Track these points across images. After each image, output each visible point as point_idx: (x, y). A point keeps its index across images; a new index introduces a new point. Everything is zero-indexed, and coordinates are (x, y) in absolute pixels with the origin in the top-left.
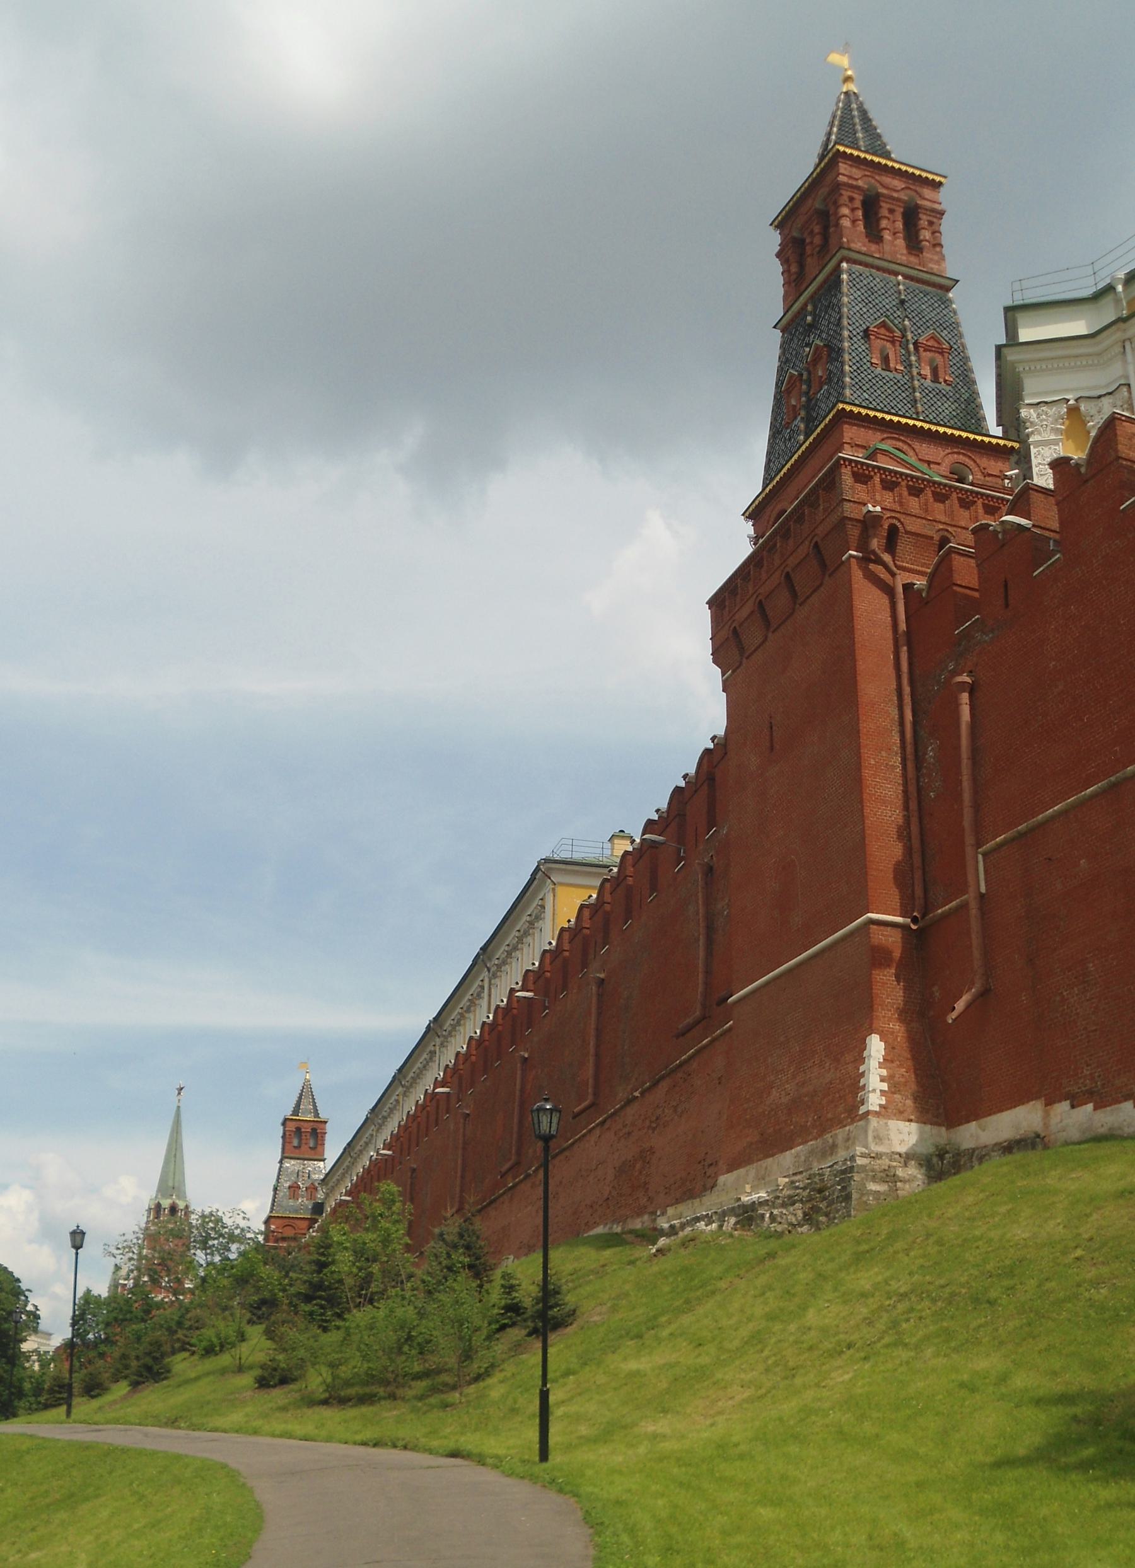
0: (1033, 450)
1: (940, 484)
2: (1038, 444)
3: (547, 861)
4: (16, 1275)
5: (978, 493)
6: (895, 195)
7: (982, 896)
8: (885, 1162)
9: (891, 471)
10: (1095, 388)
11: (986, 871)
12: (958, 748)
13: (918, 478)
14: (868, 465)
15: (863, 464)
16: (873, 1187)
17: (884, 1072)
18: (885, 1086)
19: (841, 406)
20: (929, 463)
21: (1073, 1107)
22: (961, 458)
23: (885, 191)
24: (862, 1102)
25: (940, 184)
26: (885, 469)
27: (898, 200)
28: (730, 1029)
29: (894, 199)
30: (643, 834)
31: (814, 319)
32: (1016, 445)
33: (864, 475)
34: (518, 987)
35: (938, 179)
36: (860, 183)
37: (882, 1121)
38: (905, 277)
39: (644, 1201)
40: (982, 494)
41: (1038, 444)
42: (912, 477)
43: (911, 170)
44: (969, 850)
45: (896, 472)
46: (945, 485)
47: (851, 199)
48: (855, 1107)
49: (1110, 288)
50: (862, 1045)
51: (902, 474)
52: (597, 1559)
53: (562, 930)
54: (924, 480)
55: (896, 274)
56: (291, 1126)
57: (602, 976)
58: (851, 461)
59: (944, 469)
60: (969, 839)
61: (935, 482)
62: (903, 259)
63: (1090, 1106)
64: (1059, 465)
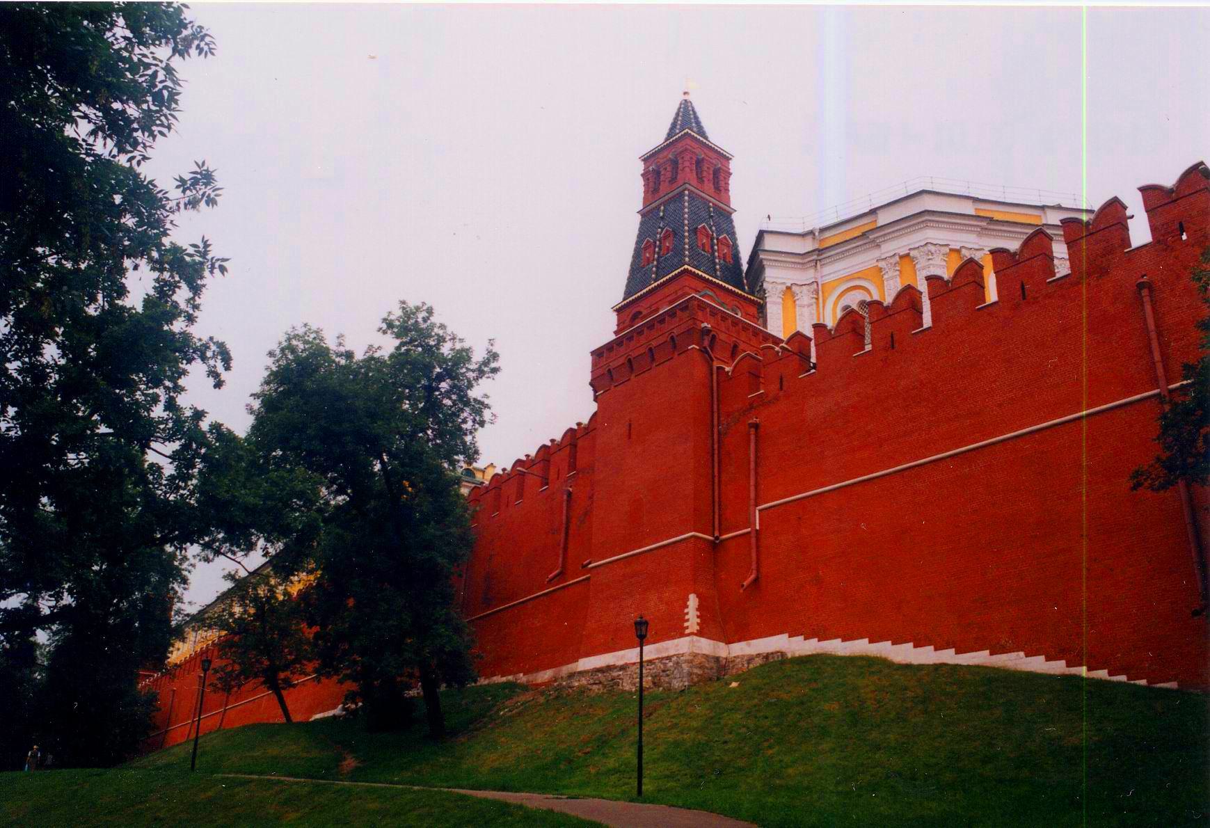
0: (768, 306)
49: (811, 233)
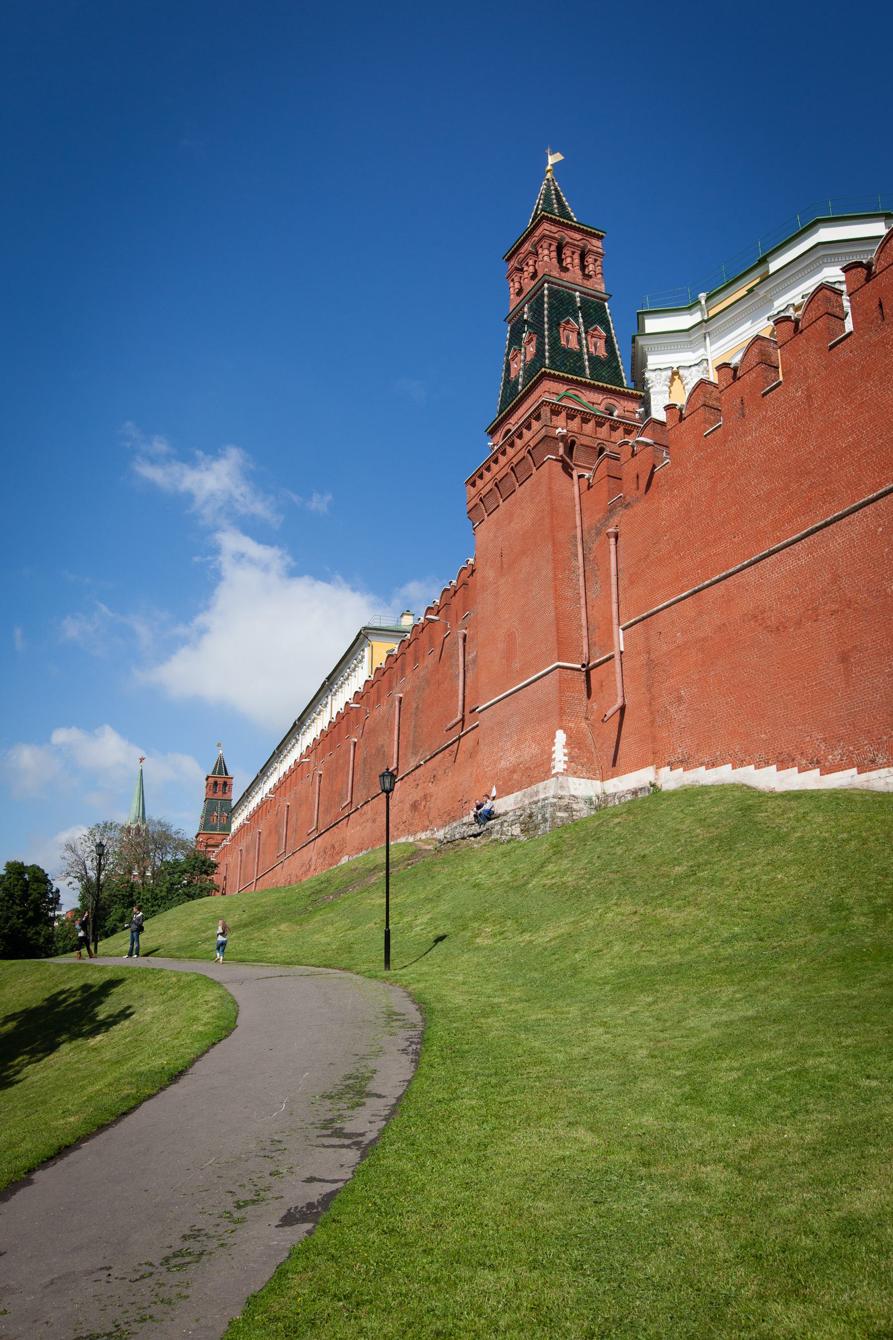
1: (600, 416)
2: (655, 393)
3: (365, 628)
4: (46, 872)
5: (621, 422)
6: (576, 243)
7: (622, 653)
8: (565, 802)
9: (572, 409)
10: (688, 361)
11: (624, 639)
12: (609, 569)
13: (587, 413)
14: (560, 405)
15: (556, 404)
16: (559, 814)
17: (566, 751)
18: (566, 759)
19: (543, 369)
20: (593, 403)
21: (671, 770)
22: (612, 401)
23: (570, 241)
24: (554, 768)
25: (602, 237)
26: (569, 408)
27: (578, 246)
28: (477, 726)
29: (575, 245)
30: (426, 615)
31: (873, 1155)
32: (643, 394)
33: (558, 411)
34: (351, 701)
35: (601, 234)
36: (556, 235)
37: (565, 778)
38: (581, 292)
39: (427, 823)
40: (624, 423)
41: (655, 393)
42: (584, 412)
43: (585, 228)
44: (615, 627)
45: (575, 410)
46: (603, 417)
47: (550, 245)
48: (550, 770)
50: (553, 736)
51: (578, 411)
52: (887, 959)
53: (378, 669)
54: (591, 414)
55: (576, 291)
56: (211, 780)
57: (401, 695)
58: (550, 403)
59: (602, 408)
60: (615, 621)
61: (597, 416)
62: (580, 281)
63: (681, 769)
64: (669, 408)
